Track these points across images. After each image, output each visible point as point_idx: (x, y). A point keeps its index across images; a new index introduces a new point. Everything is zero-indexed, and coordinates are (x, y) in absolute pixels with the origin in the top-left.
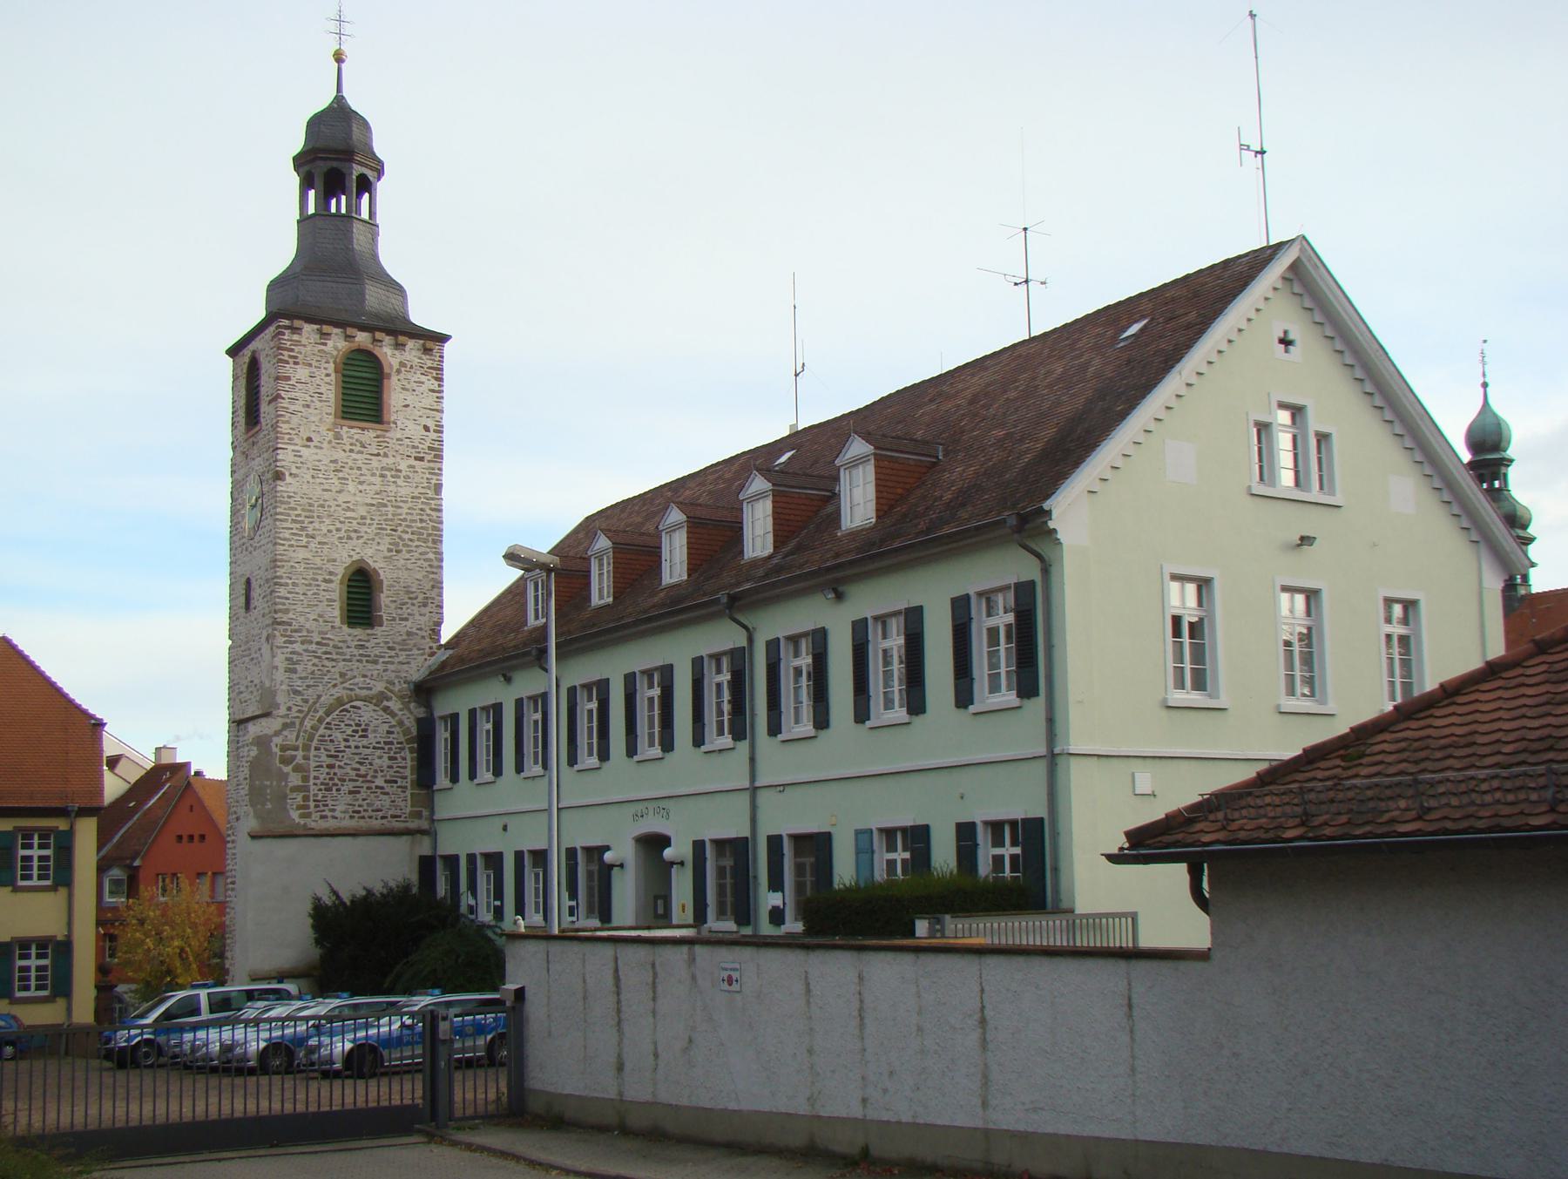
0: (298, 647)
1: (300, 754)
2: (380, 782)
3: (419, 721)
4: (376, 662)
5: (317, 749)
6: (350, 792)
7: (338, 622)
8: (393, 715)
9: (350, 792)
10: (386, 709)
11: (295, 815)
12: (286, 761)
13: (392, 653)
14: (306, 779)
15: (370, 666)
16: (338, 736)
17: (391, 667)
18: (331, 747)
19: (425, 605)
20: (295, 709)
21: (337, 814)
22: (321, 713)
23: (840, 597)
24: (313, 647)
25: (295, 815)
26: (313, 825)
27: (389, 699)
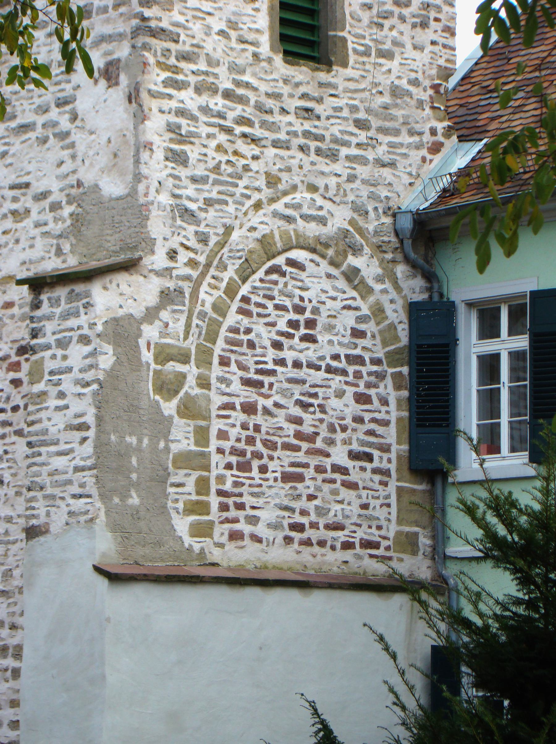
0: (189, 99)
1: (191, 371)
2: (339, 455)
3: (414, 309)
4: (333, 156)
5: (224, 362)
6: (287, 477)
7: (265, 49)
8: (365, 290)
9: (287, 477)
10: (352, 275)
11: (182, 525)
12: (168, 387)
13: (362, 136)
14: (202, 436)
15: (323, 165)
16: (263, 334)
17: (363, 171)
18: (249, 361)
19: (424, 25)
20: (183, 256)
21: (261, 530)
22: (230, 273)
23: (147, 309)
24: (218, 103)
25: (182, 525)
26: (216, 555)
27: (356, 251)
